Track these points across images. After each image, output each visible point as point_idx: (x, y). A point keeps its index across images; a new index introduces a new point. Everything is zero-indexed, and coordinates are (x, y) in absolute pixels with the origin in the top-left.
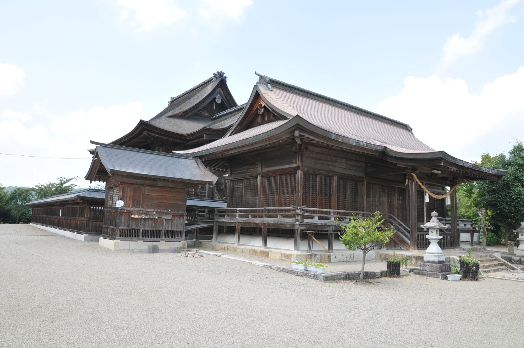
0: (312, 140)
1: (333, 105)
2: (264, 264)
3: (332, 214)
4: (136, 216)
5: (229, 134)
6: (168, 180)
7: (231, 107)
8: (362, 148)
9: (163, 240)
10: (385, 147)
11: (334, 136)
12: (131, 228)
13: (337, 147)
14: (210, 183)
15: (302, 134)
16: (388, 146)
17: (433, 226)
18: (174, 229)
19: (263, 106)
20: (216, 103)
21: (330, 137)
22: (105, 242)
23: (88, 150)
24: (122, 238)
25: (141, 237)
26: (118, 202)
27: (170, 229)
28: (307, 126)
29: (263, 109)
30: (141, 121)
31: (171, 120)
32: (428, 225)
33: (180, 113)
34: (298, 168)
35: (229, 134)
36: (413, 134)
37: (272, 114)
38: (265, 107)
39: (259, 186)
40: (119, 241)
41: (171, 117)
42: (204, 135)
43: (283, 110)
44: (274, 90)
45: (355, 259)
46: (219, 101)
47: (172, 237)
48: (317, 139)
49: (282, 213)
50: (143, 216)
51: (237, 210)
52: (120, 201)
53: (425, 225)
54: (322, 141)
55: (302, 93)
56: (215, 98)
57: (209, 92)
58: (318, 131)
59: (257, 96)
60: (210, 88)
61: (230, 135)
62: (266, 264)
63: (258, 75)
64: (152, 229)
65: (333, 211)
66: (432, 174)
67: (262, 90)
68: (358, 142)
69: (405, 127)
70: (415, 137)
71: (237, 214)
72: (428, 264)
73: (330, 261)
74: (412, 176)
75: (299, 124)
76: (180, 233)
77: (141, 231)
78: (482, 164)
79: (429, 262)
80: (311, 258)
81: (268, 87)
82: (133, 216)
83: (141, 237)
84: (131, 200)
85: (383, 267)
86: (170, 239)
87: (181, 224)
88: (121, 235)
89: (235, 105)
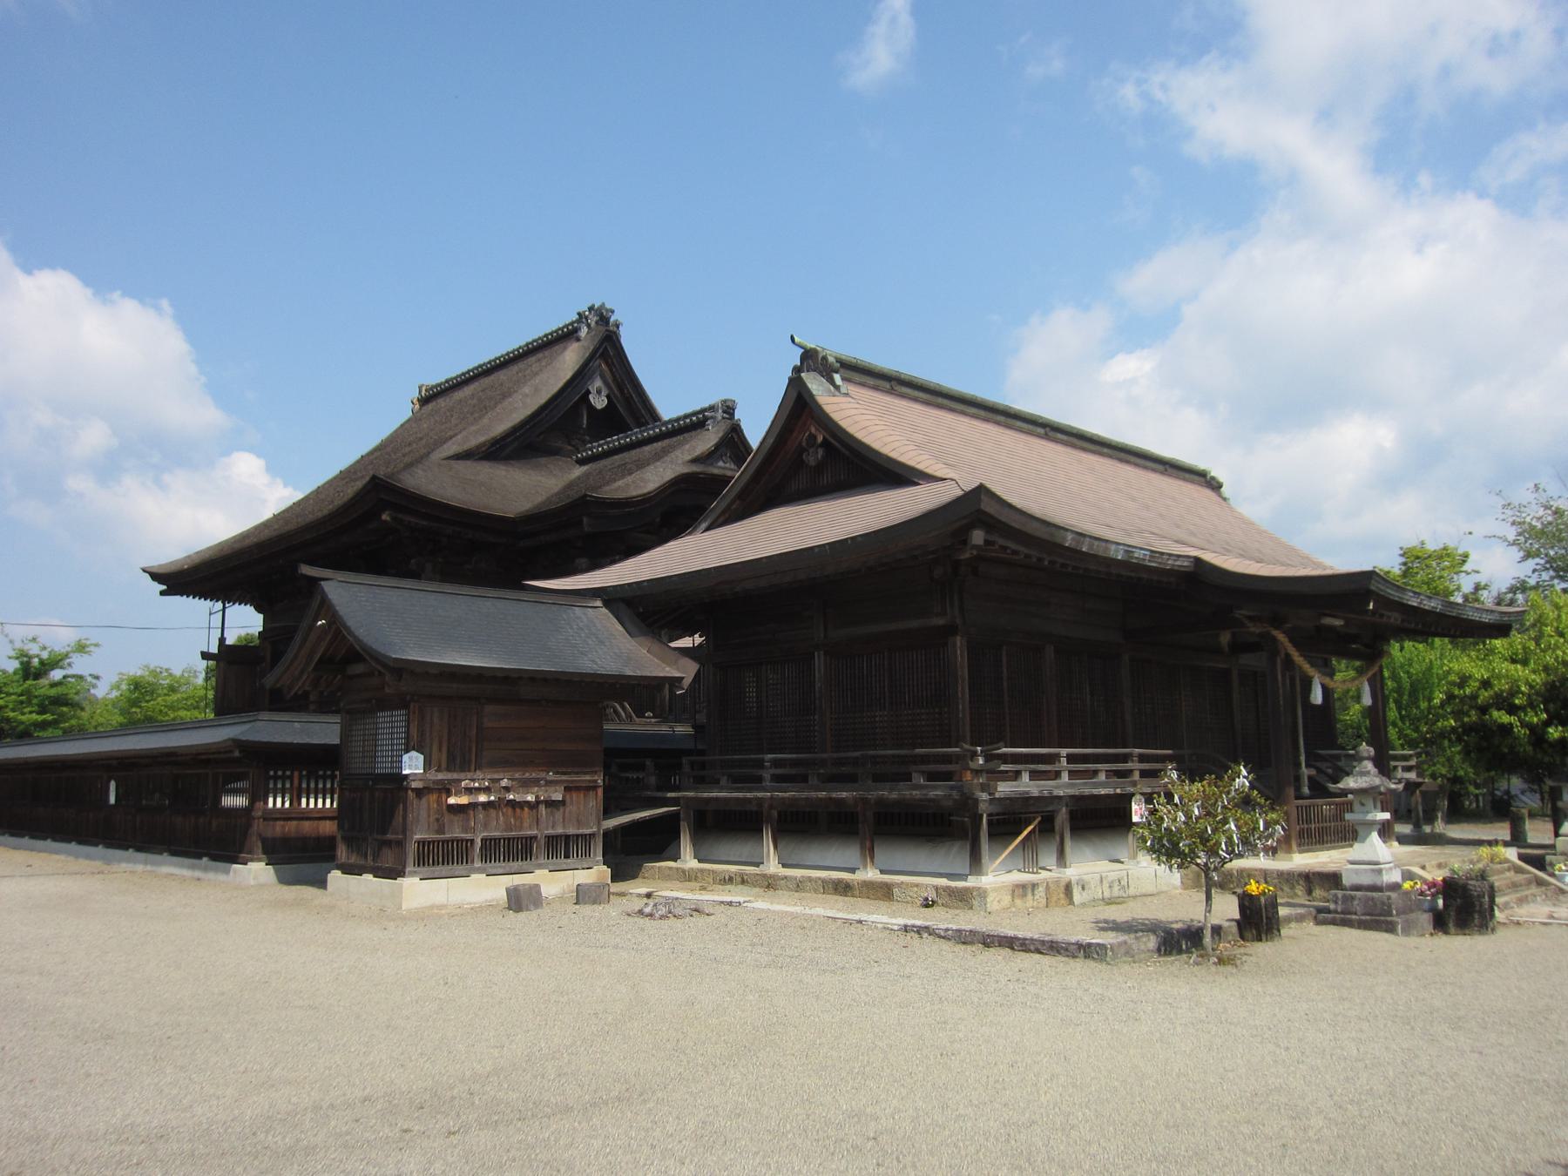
0: (1015, 552)
1: (1046, 437)
2: (902, 921)
3: (1064, 760)
4: (464, 800)
5: (704, 526)
6: (545, 680)
7: (641, 424)
8: (1140, 567)
9: (540, 867)
10: (1198, 560)
11: (1070, 536)
12: (447, 836)
13: (1075, 568)
14: (675, 682)
15: (991, 538)
16: (1207, 557)
17: (1364, 785)
18: (572, 831)
19: (820, 439)
20: (591, 407)
21: (1058, 540)
22: (418, 891)
23: (156, 577)
24: (425, 870)
25: (478, 864)
26: (406, 758)
27: (560, 831)
28: (1004, 516)
29: (821, 452)
30: (374, 478)
31: (461, 466)
32: (1351, 783)
33: (483, 444)
34: (951, 630)
35: (704, 526)
36: (1225, 499)
37: (867, 470)
38: (825, 443)
39: (818, 685)
40: (416, 880)
41: (458, 457)
42: (585, 520)
43: (894, 455)
44: (852, 389)
45: (1132, 891)
46: (599, 402)
47: (567, 857)
48: (1026, 551)
49: (924, 768)
50: (483, 798)
51: (763, 760)
52: (414, 754)
53: (1341, 785)
54: (1026, 551)
55: (982, 413)
56: (588, 392)
57: (569, 375)
58: (1031, 528)
59: (798, 407)
60: (570, 359)
61: (707, 529)
62: (910, 922)
63: (1220, 495)
64: (506, 834)
65: (1064, 752)
66: (1320, 629)
67: (815, 385)
68: (1129, 549)
69: (1215, 486)
70: (1232, 510)
71: (767, 775)
72: (1358, 894)
73: (1071, 902)
74: (1274, 639)
75: (977, 509)
76: (588, 839)
77: (478, 842)
78: (1405, 574)
79: (1358, 888)
80: (1024, 895)
81: (832, 382)
82: (452, 801)
83: (478, 864)
84: (445, 749)
85: (1226, 908)
86: (562, 862)
87: (588, 816)
88: (421, 860)
89: (655, 416)
